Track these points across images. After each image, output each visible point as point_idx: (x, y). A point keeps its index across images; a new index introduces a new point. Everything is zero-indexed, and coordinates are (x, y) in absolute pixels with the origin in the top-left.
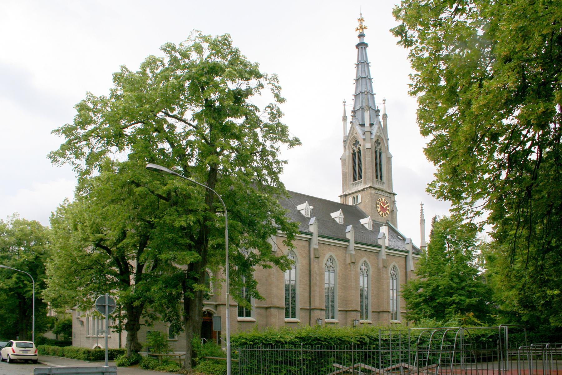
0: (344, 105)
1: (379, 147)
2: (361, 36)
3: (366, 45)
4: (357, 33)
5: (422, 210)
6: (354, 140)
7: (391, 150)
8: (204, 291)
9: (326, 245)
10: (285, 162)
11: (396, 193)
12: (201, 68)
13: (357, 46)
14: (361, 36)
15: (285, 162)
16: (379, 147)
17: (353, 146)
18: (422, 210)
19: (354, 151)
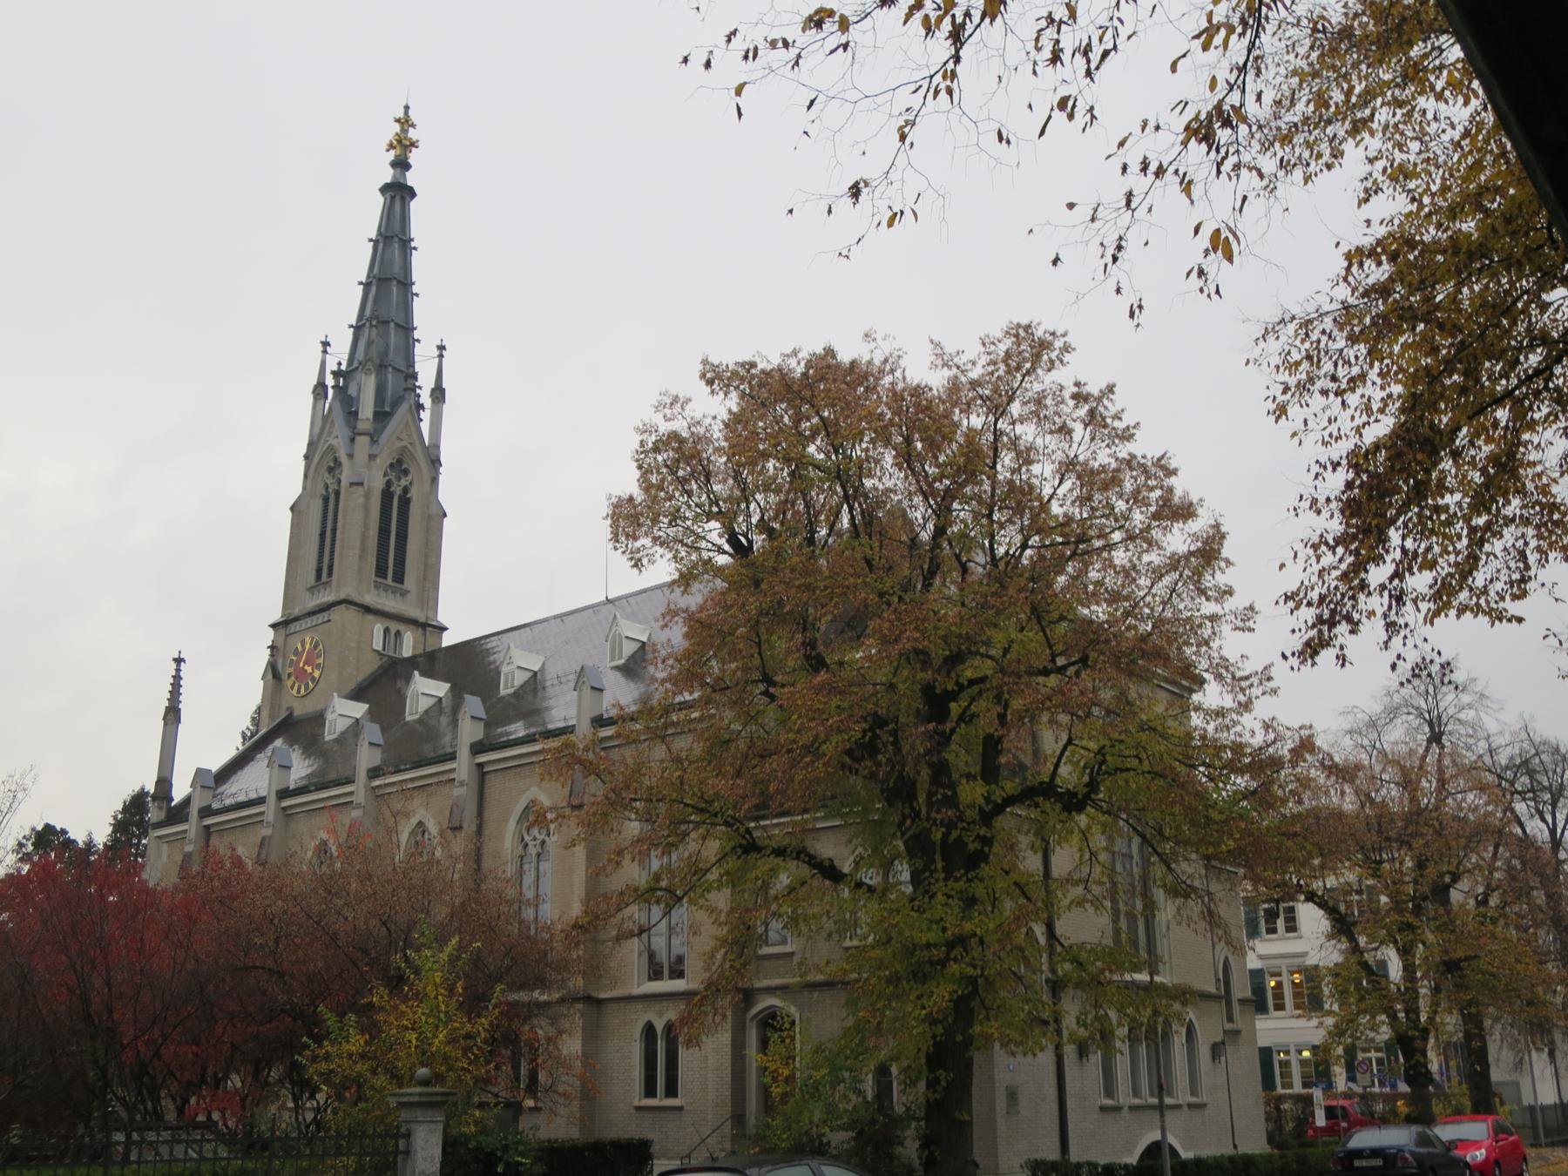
0: (325, 352)
1: (403, 482)
2: (401, 164)
3: (411, 193)
4: (392, 155)
5: (177, 678)
6: (330, 457)
7: (447, 493)
8: (1246, 745)
9: (527, 768)
10: (1342, 660)
11: (447, 625)
12: (1356, 616)
13: (385, 189)
14: (401, 164)
15: (1342, 660)
16: (403, 482)
17: (326, 475)
18: (177, 678)
19: (327, 487)
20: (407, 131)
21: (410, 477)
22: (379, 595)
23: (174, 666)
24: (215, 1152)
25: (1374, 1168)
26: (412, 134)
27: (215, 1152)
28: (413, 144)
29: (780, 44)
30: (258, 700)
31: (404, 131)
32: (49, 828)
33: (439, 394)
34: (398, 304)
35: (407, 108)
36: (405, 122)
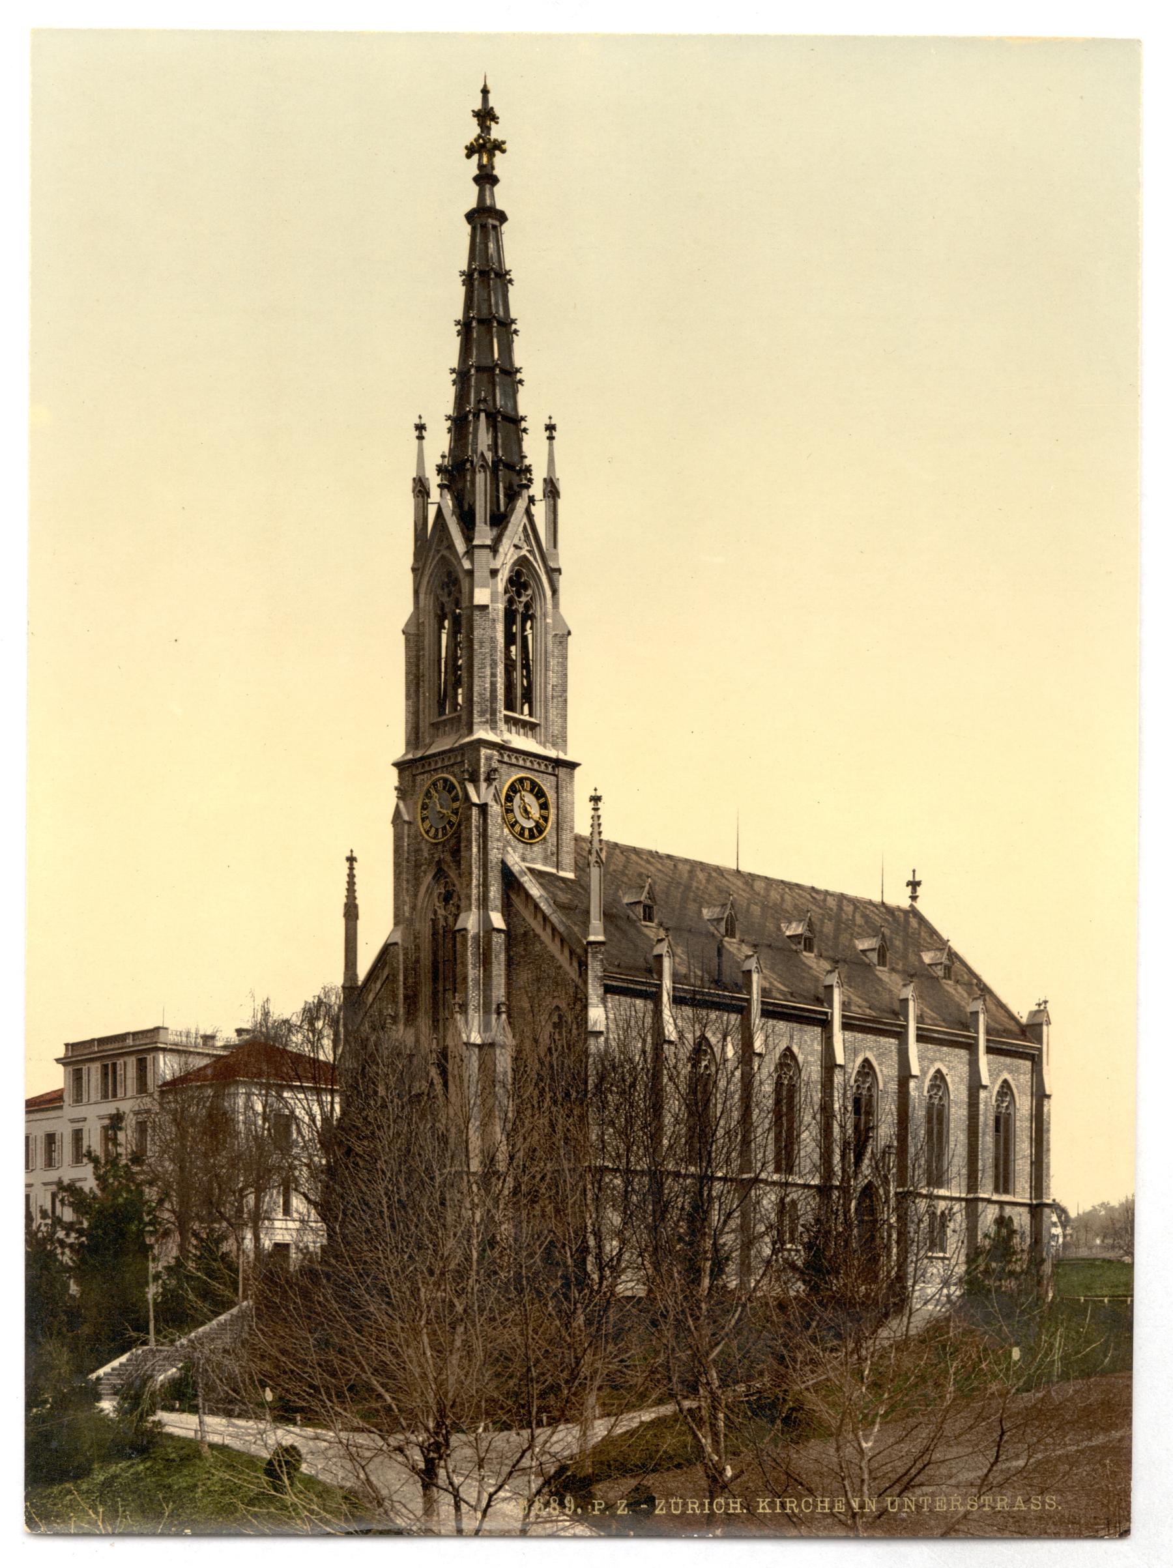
2: (486, 179)
3: (502, 217)
5: (351, 876)
13: (470, 217)
14: (486, 179)
18: (351, 876)
20: (489, 128)
21: (529, 592)
22: (510, 731)
23: (347, 864)
24: (506, 1465)
25: (102, 1365)
26: (496, 133)
27: (506, 1465)
28: (499, 146)
29: (542, 800)
30: (406, 608)
31: (485, 128)
32: (71, 1047)
33: (552, 491)
34: (470, 841)
35: (485, 92)
36: (485, 116)
